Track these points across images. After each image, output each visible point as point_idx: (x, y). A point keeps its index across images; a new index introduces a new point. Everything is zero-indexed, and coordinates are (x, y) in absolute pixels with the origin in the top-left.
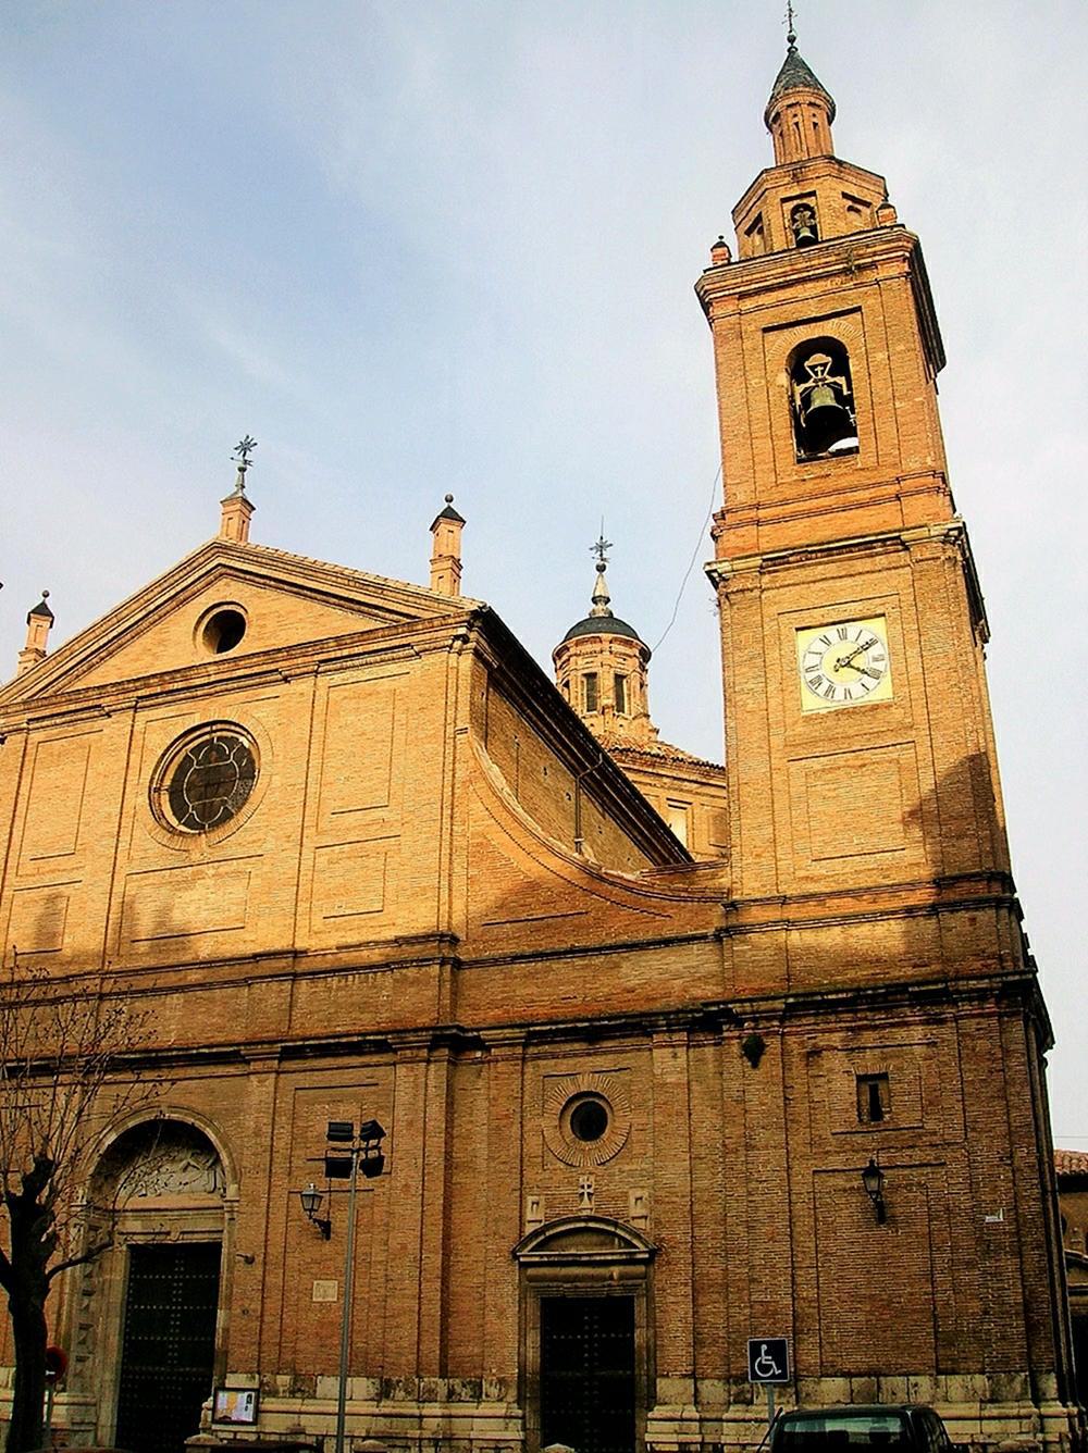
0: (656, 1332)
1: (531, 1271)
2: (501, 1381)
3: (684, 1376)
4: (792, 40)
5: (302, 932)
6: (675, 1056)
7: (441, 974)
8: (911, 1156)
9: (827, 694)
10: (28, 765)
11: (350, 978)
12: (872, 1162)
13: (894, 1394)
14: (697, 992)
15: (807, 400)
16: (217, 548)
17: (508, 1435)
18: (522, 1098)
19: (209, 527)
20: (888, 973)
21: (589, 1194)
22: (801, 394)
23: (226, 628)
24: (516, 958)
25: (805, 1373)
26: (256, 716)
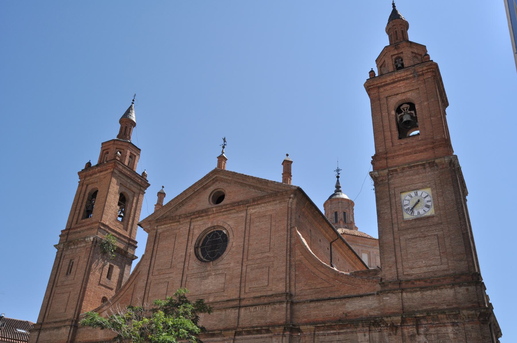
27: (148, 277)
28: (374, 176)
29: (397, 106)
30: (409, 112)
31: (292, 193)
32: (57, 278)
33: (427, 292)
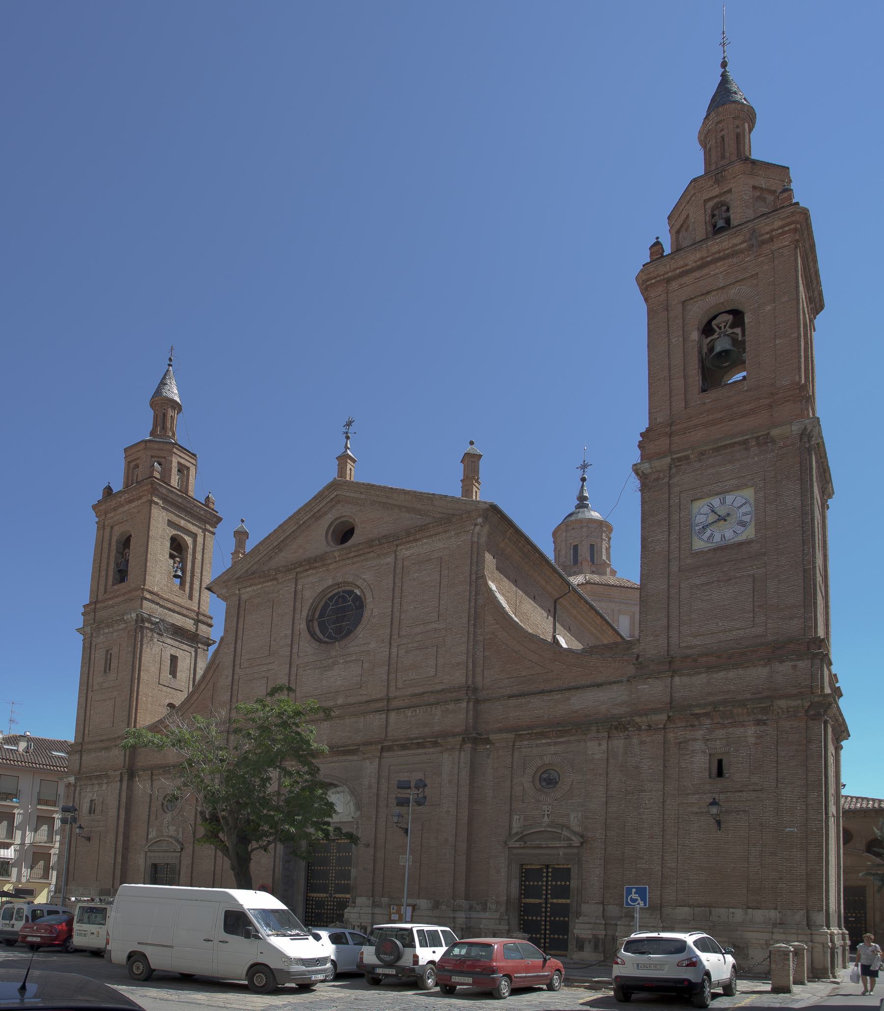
0: (582, 882)
1: (515, 851)
2: (497, 902)
3: (596, 903)
4: (724, 65)
5: (392, 689)
6: (600, 745)
7: (468, 707)
8: (740, 796)
9: (709, 538)
10: (242, 613)
11: (418, 711)
12: (714, 799)
13: (719, 917)
14: (615, 712)
15: (711, 349)
16: (333, 486)
17: (501, 927)
18: (512, 768)
19: (332, 474)
20: (735, 698)
21: (548, 814)
22: (708, 344)
23: (344, 534)
24: (510, 697)
25: (667, 904)
26: (363, 577)
27: (234, 671)
28: (643, 472)
29: (705, 321)
30: (730, 331)
31: (479, 516)
32: (91, 678)
33: (718, 674)
